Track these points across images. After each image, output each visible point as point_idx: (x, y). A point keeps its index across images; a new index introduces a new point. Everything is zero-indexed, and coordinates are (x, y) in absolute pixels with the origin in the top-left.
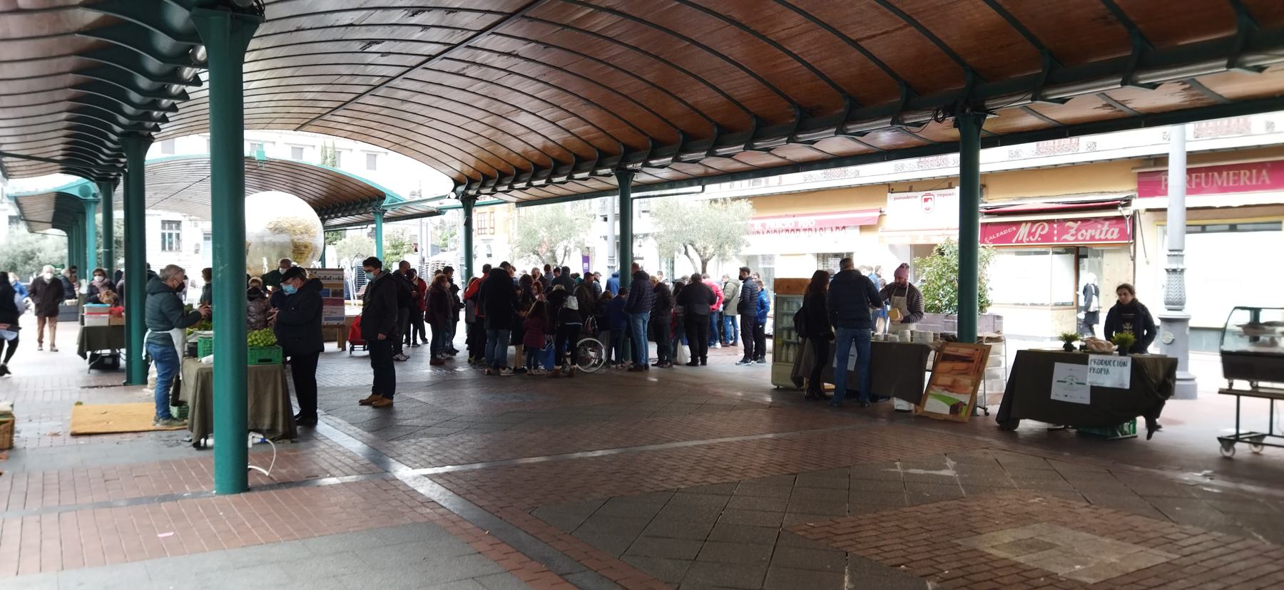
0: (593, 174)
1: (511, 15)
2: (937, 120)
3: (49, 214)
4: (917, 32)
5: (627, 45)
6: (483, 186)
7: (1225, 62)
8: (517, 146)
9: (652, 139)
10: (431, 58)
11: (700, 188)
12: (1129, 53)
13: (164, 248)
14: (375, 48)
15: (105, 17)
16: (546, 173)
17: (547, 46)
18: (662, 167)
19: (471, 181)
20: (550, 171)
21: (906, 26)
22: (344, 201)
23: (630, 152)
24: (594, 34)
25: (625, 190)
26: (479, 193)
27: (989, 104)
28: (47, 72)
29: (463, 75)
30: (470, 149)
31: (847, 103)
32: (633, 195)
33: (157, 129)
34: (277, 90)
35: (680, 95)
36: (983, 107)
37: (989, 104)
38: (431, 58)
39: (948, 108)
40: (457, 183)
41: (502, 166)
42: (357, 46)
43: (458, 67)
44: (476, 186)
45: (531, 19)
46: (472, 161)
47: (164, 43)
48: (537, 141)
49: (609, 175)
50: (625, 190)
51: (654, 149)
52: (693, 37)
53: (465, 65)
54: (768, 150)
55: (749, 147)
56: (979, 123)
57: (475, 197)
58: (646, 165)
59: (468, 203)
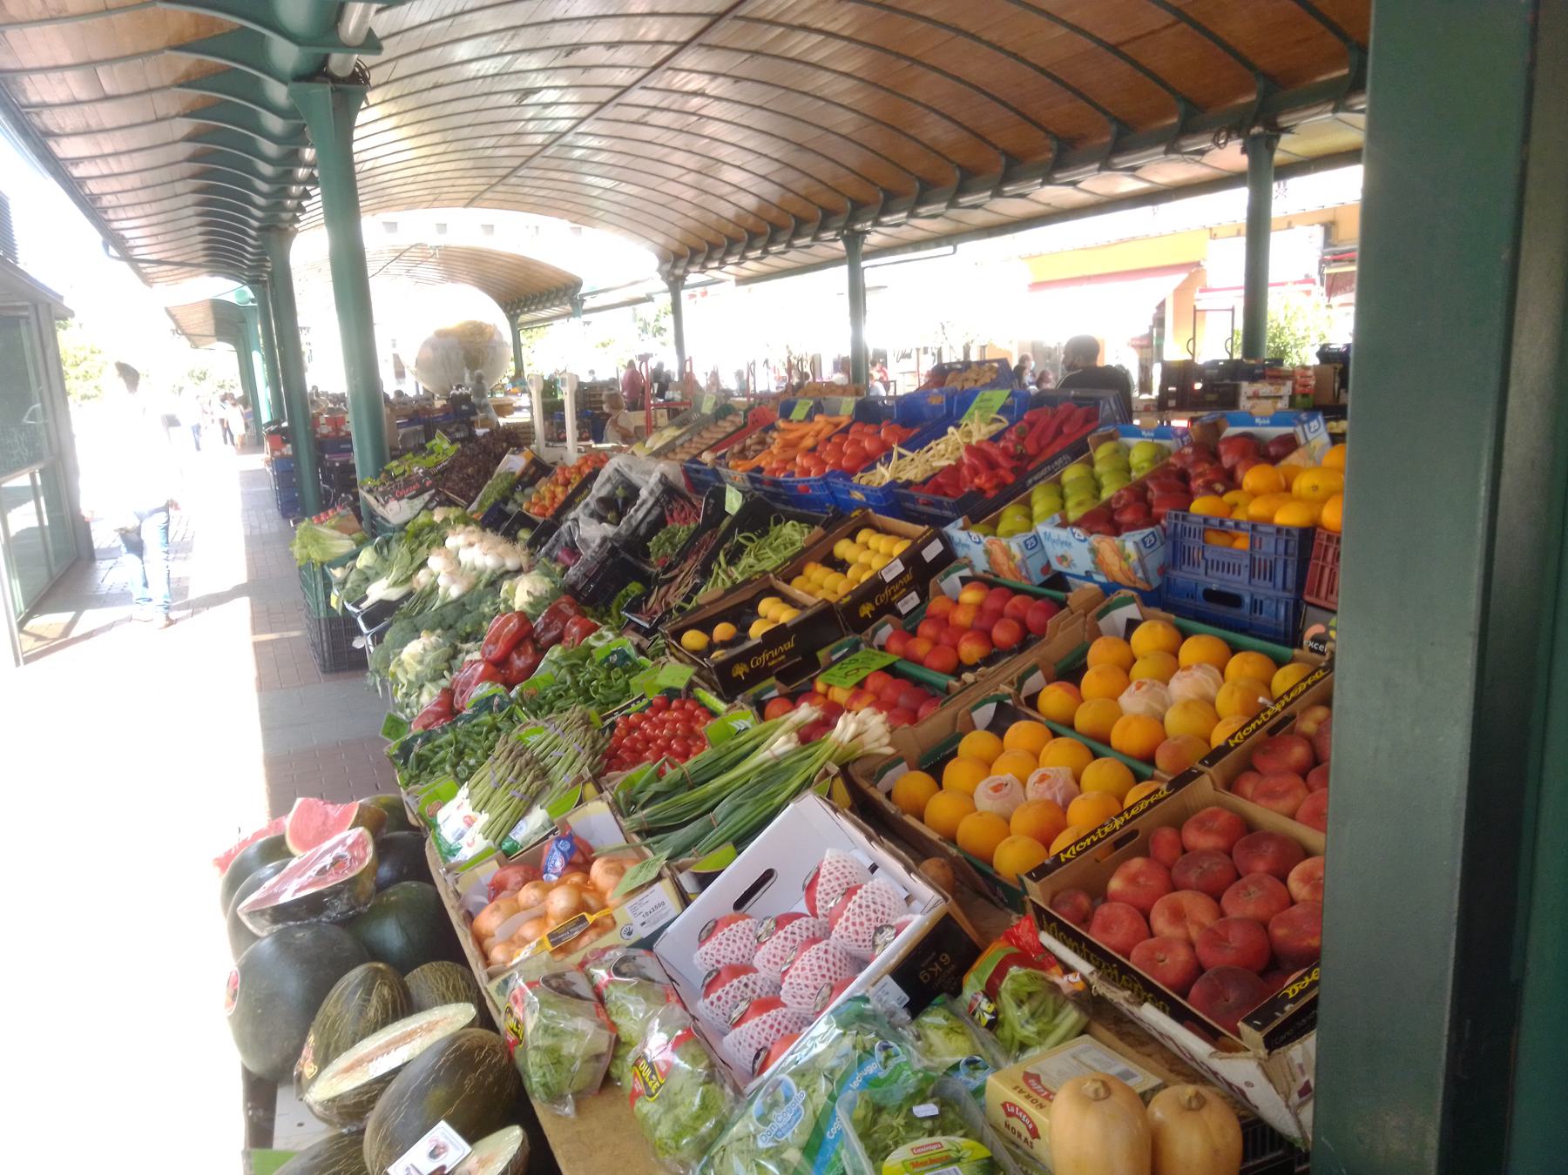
0: (816, 239)
1: (685, 44)
2: (1218, 145)
3: (209, 328)
4: (1190, 29)
5: (834, 71)
6: (691, 262)
7: (1331, 107)
8: (728, 211)
9: (821, 208)
10: (602, 105)
11: (950, 249)
12: (1345, 71)
13: (18, 664)
14: (533, 99)
15: (200, 62)
16: (761, 242)
17: (737, 79)
18: (934, 216)
19: (678, 257)
20: (744, 244)
21: (1174, 24)
22: (531, 293)
23: (858, 209)
24: (792, 60)
25: (854, 254)
26: (687, 272)
27: (1284, 120)
28: (147, 144)
29: (645, 124)
30: (674, 217)
31: (1114, 128)
32: (863, 264)
33: (302, 210)
34: (432, 160)
35: (912, 132)
36: (1275, 124)
37: (1284, 120)
38: (602, 105)
39: (1235, 126)
40: (664, 260)
41: (711, 236)
42: (510, 99)
43: (636, 114)
44: (683, 263)
45: (711, 47)
46: (677, 233)
47: (279, 92)
48: (749, 202)
49: (835, 240)
50: (854, 254)
51: (889, 202)
52: (913, 54)
53: (645, 111)
54: (1074, 184)
55: (997, 193)
56: (1271, 148)
57: (683, 278)
58: (877, 223)
59: (676, 284)
